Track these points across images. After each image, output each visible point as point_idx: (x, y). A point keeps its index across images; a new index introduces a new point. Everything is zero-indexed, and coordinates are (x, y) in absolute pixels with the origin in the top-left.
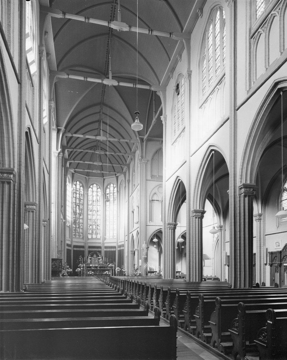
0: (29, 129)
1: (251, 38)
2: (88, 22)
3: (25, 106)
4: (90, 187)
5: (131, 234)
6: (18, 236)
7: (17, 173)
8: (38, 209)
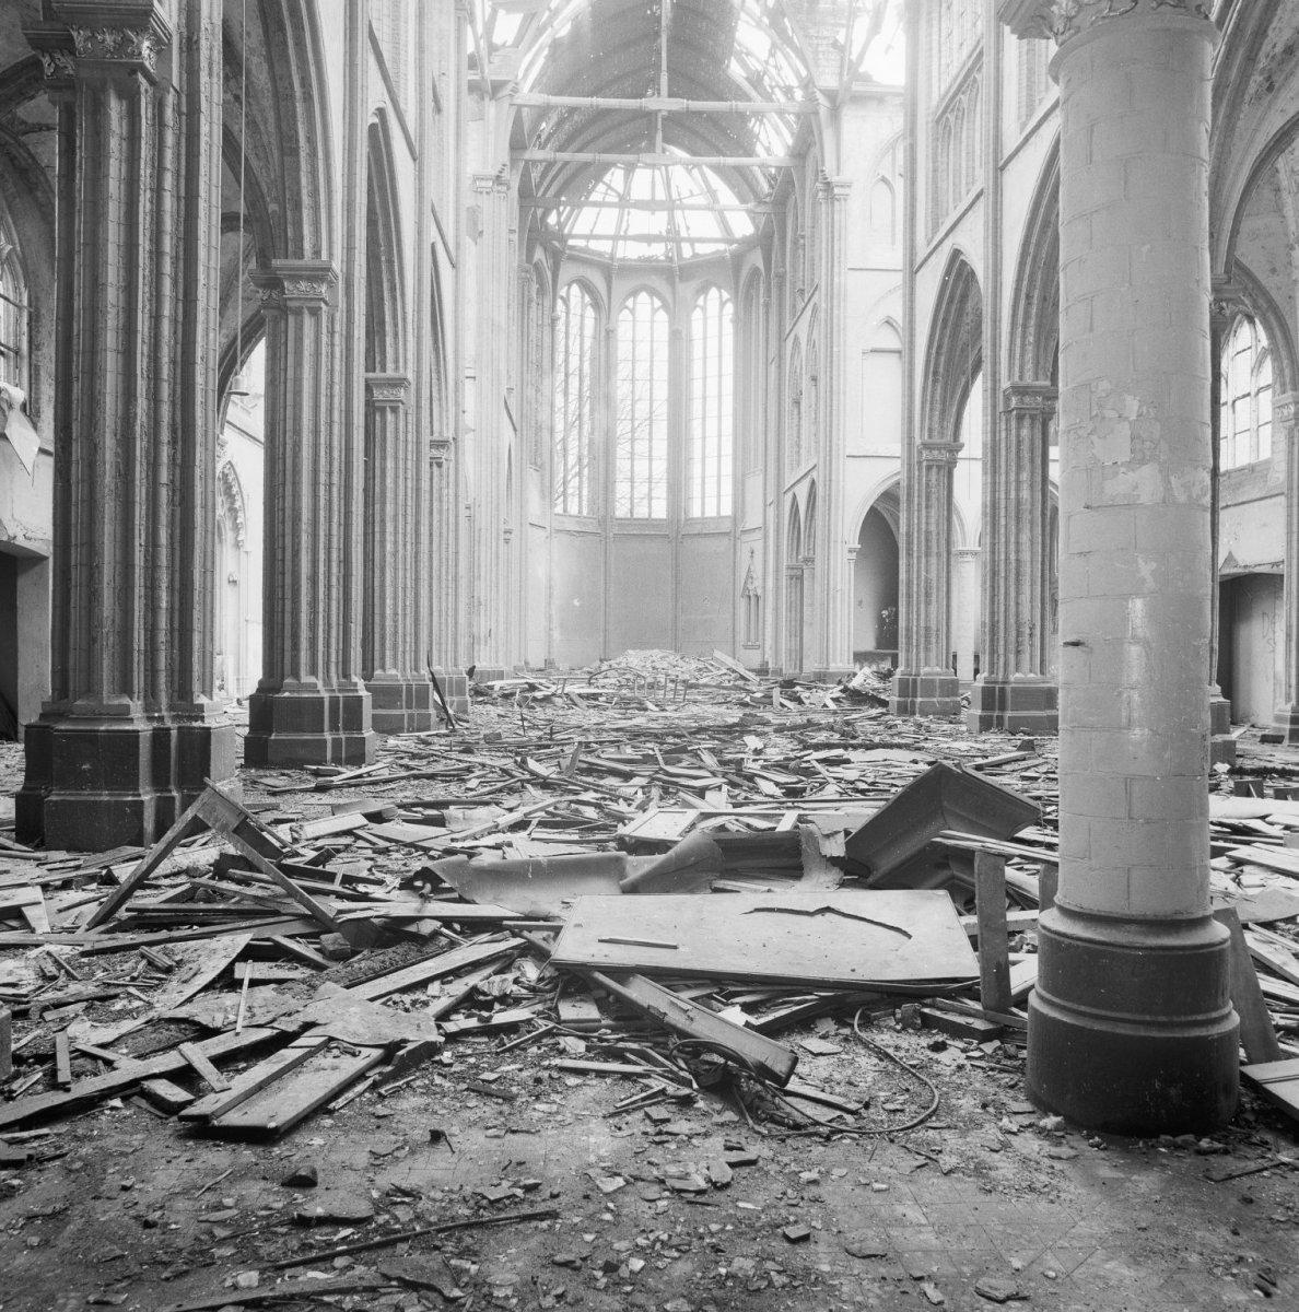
0: (381, 112)
3: (366, 35)
5: (790, 495)
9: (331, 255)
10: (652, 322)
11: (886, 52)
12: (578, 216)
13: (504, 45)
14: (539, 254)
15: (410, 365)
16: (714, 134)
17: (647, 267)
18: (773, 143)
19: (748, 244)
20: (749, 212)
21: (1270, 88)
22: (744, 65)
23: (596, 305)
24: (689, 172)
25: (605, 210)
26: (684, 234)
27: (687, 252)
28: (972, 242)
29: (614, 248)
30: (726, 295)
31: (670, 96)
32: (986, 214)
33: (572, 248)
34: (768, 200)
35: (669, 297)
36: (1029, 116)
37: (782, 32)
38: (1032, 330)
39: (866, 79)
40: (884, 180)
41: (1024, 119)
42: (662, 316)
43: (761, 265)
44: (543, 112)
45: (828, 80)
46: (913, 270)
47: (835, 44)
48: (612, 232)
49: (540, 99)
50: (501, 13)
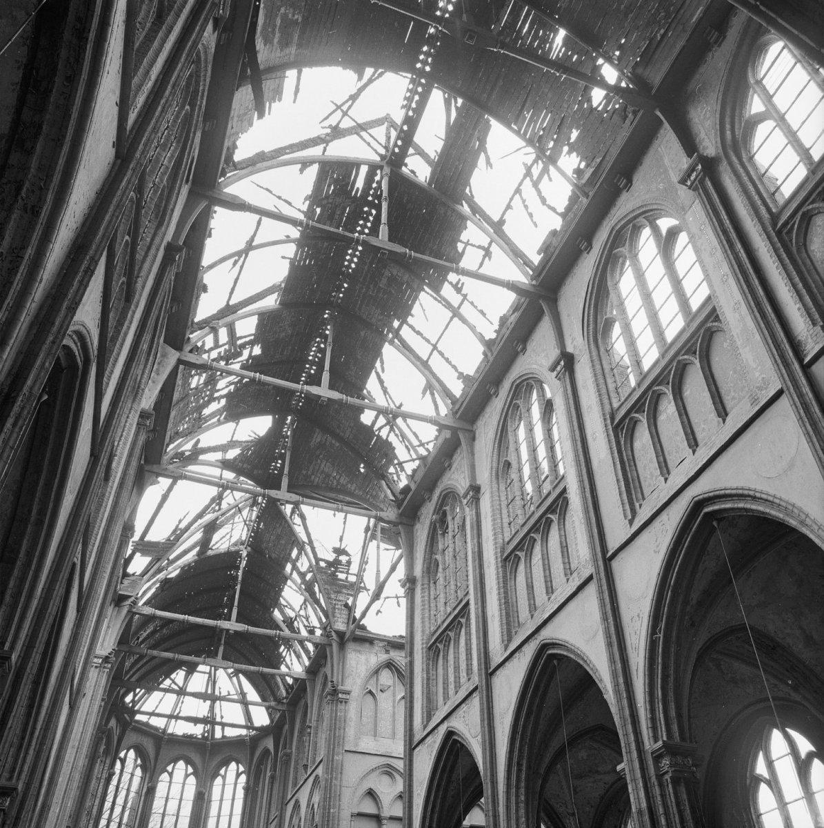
1: (563, 476)
2: (224, 737)
4: (165, 770)
6: (137, 131)
7: (13, 668)
8: (14, 813)
9: (12, 648)
10: (184, 784)
11: (377, 614)
12: (147, 699)
13: (133, 575)
14: (113, 723)
15: (23, 776)
16: (255, 653)
17: (188, 740)
18: (294, 665)
19: (263, 731)
20: (267, 708)
21: (693, 625)
22: (282, 613)
23: (144, 768)
24: (230, 678)
25: (168, 695)
26: (218, 719)
27: (218, 735)
28: (468, 726)
29: (167, 725)
30: (241, 769)
31: (237, 621)
32: (481, 704)
33: (138, 722)
34: (285, 701)
35: (200, 767)
36: (510, 640)
37: (312, 594)
38: (522, 791)
39: (363, 628)
40: (370, 692)
41: (506, 642)
42: (192, 780)
43: (271, 746)
44: (150, 619)
45: (340, 626)
46: (412, 747)
47: (346, 605)
48: (168, 712)
49: (148, 611)
50: (138, 555)
